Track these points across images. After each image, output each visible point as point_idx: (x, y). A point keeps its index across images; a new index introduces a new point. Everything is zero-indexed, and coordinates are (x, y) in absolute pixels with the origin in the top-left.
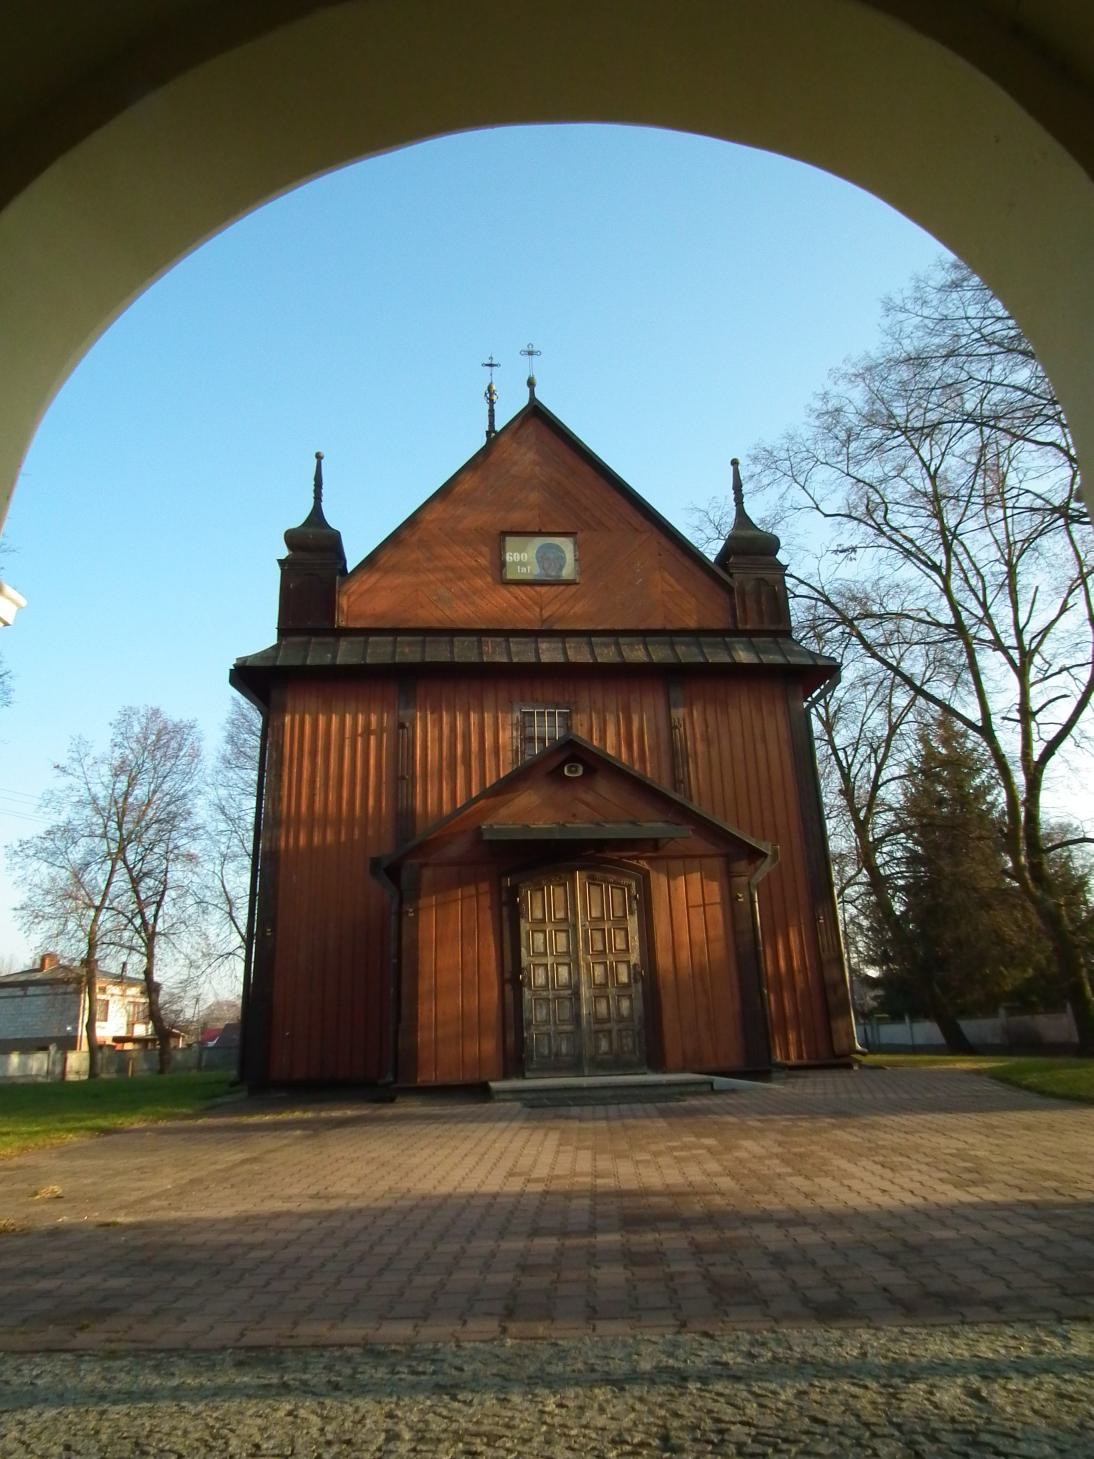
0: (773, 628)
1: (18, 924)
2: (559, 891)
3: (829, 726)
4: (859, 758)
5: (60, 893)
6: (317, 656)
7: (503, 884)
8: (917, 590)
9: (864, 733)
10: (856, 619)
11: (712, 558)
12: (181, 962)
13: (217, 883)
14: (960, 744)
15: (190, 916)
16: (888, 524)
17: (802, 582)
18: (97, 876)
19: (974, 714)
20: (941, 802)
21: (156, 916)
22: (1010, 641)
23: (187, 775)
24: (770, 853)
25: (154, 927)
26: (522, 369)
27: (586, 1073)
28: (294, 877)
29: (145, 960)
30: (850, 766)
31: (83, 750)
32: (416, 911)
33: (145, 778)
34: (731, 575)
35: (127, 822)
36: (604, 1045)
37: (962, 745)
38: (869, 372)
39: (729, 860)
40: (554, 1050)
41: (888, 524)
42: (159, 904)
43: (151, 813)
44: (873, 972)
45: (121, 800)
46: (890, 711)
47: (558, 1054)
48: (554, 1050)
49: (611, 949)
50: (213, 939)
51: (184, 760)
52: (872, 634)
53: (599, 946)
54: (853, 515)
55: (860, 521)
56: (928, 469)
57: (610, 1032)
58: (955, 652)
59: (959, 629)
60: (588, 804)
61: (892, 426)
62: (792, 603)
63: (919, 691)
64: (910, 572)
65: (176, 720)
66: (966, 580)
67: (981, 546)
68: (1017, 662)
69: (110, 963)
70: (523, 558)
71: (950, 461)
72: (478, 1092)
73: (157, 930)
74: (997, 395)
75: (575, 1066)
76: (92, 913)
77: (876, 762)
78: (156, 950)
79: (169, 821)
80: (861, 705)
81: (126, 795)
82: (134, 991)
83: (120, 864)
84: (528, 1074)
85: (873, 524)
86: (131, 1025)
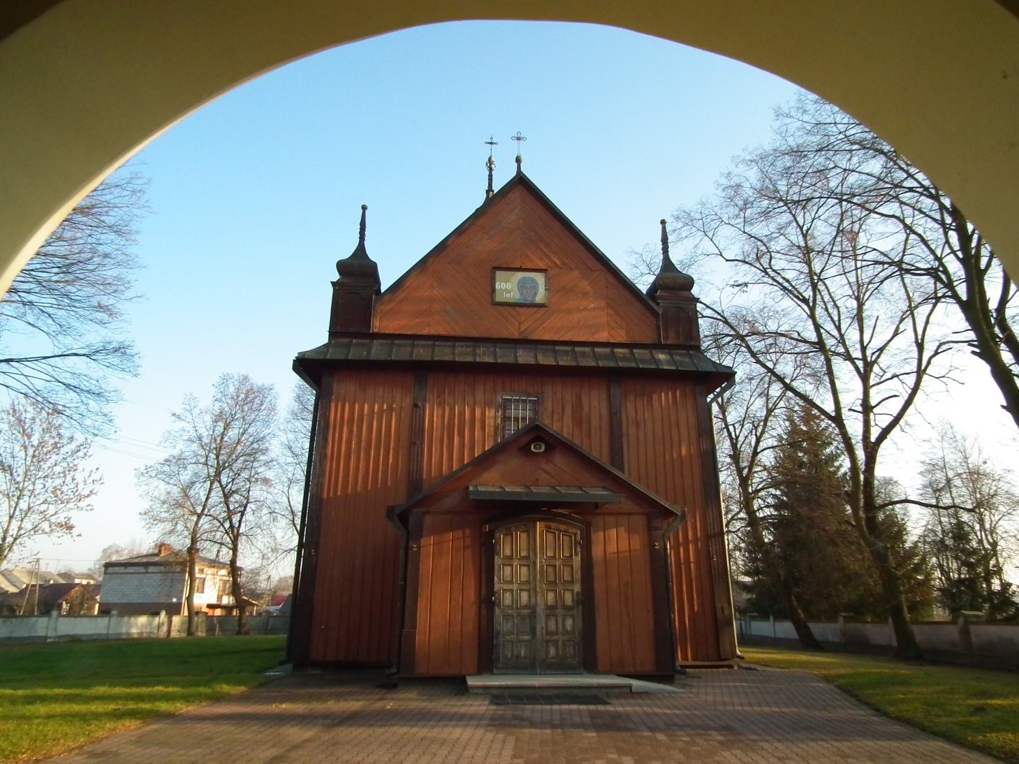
0: (687, 343)
1: (143, 523)
2: (524, 535)
3: (723, 409)
4: (745, 432)
5: (173, 503)
6: (356, 353)
7: (483, 531)
8: (793, 317)
9: (748, 418)
10: (747, 335)
11: (644, 292)
12: (257, 555)
13: (285, 500)
14: (815, 423)
15: (264, 523)
16: (771, 268)
17: (708, 307)
18: (200, 491)
19: (829, 407)
20: (802, 464)
21: (240, 522)
22: (856, 354)
23: (267, 423)
24: (679, 514)
25: (238, 531)
26: (513, 150)
27: (538, 672)
28: (333, 513)
29: (231, 552)
30: (737, 437)
31: (193, 403)
32: (419, 547)
33: (236, 424)
34: (658, 304)
35: (223, 454)
36: (552, 651)
37: (818, 425)
38: (761, 159)
39: (649, 517)
40: (515, 653)
41: (771, 268)
42: (243, 514)
43: (239, 448)
44: (747, 579)
45: (219, 439)
46: (768, 399)
47: (518, 657)
48: (515, 653)
49: (560, 579)
50: (279, 540)
51: (264, 413)
52: (757, 345)
53: (551, 578)
54: (747, 260)
55: (751, 264)
56: (801, 228)
57: (557, 641)
58: (818, 362)
59: (820, 345)
60: (548, 473)
61: (774, 196)
62: (701, 321)
63: (788, 387)
64: (788, 303)
65: (260, 384)
66: (826, 309)
67: (838, 287)
68: (862, 370)
69: (208, 550)
70: (508, 287)
71: (818, 223)
72: (457, 685)
73: (241, 531)
74: (852, 178)
75: (530, 667)
76: (195, 518)
77: (756, 435)
78: (239, 546)
79: (252, 455)
80: (747, 396)
81: (223, 435)
82: (224, 572)
83: (216, 484)
84: (495, 671)
85: (761, 268)
86: (220, 598)
